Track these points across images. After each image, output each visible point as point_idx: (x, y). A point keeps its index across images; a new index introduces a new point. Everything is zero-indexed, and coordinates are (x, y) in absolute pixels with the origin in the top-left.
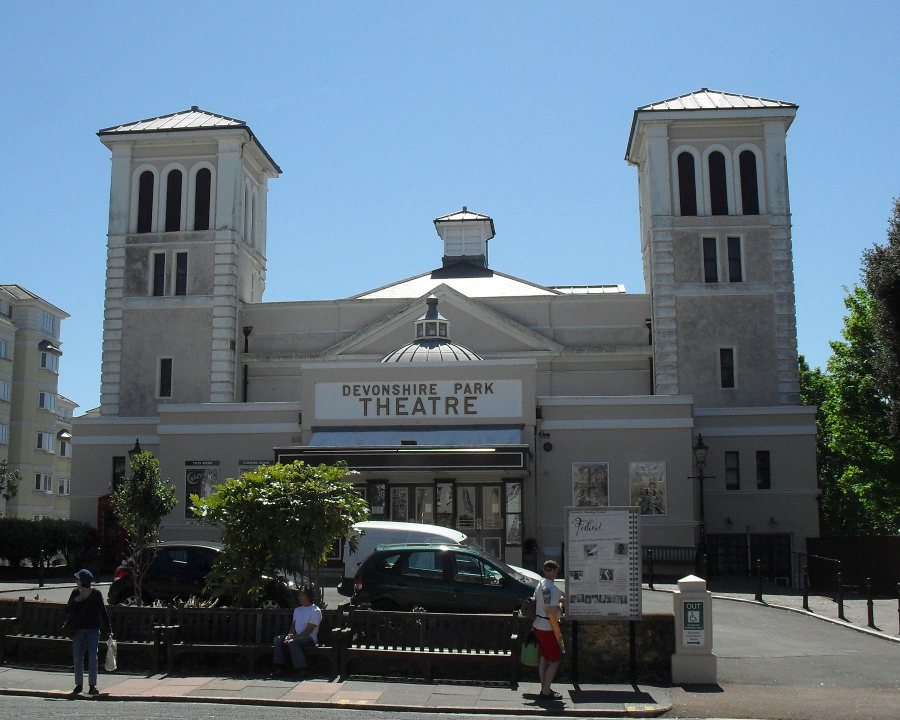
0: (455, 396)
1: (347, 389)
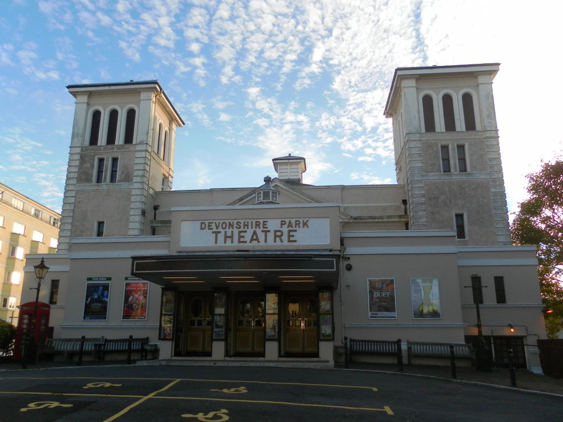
0: (281, 229)
1: (203, 225)
